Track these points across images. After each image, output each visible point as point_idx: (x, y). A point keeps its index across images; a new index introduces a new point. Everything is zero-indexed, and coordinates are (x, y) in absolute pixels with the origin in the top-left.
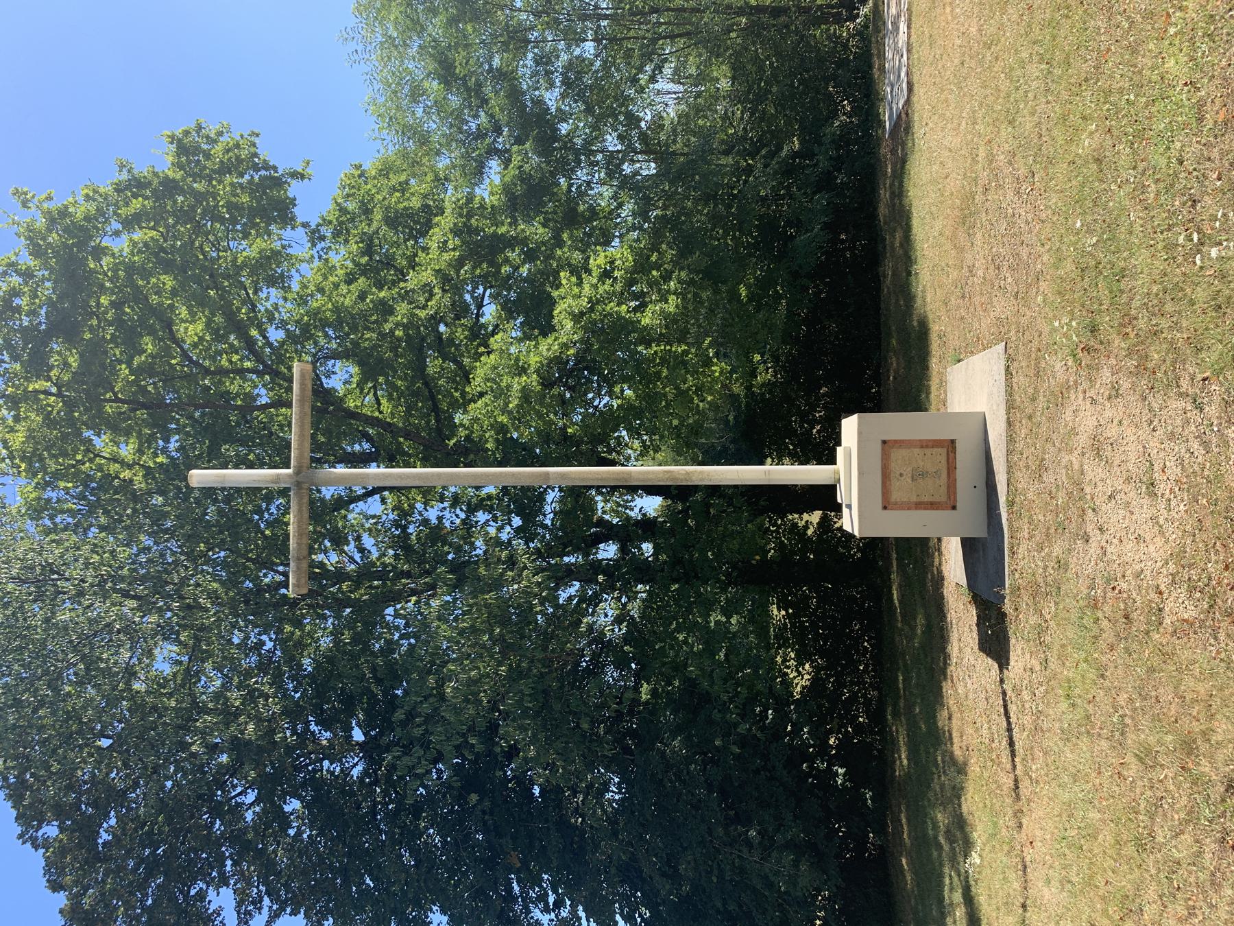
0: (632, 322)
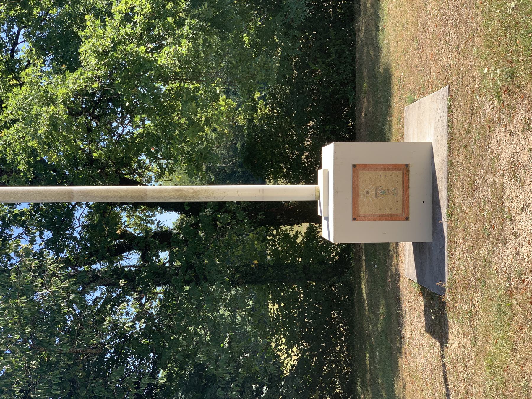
0: (150, 61)
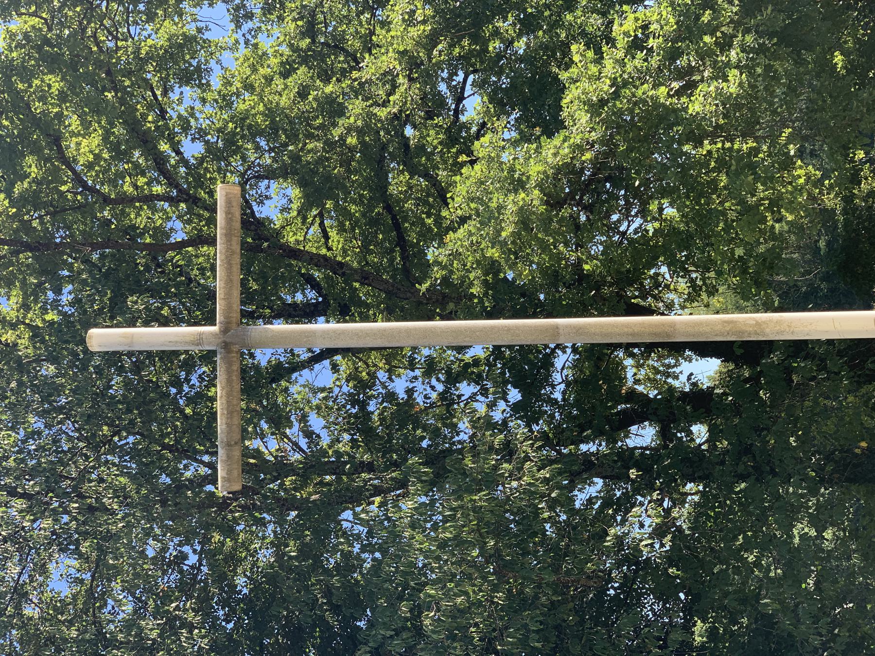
0: (675, 111)
